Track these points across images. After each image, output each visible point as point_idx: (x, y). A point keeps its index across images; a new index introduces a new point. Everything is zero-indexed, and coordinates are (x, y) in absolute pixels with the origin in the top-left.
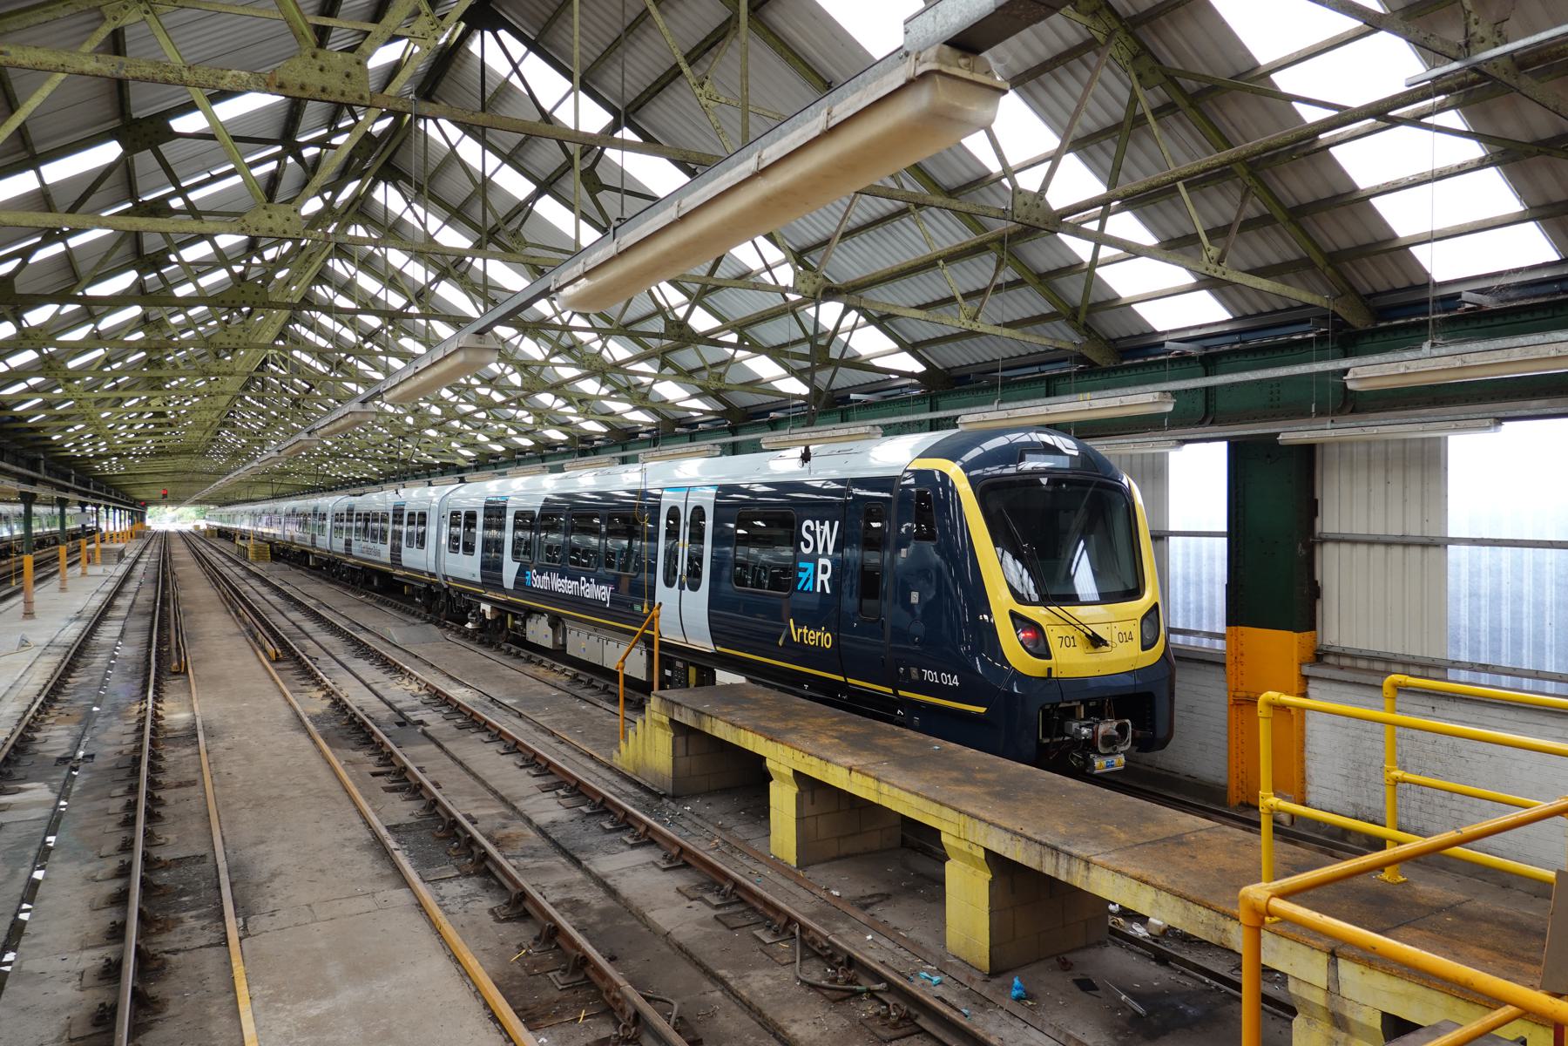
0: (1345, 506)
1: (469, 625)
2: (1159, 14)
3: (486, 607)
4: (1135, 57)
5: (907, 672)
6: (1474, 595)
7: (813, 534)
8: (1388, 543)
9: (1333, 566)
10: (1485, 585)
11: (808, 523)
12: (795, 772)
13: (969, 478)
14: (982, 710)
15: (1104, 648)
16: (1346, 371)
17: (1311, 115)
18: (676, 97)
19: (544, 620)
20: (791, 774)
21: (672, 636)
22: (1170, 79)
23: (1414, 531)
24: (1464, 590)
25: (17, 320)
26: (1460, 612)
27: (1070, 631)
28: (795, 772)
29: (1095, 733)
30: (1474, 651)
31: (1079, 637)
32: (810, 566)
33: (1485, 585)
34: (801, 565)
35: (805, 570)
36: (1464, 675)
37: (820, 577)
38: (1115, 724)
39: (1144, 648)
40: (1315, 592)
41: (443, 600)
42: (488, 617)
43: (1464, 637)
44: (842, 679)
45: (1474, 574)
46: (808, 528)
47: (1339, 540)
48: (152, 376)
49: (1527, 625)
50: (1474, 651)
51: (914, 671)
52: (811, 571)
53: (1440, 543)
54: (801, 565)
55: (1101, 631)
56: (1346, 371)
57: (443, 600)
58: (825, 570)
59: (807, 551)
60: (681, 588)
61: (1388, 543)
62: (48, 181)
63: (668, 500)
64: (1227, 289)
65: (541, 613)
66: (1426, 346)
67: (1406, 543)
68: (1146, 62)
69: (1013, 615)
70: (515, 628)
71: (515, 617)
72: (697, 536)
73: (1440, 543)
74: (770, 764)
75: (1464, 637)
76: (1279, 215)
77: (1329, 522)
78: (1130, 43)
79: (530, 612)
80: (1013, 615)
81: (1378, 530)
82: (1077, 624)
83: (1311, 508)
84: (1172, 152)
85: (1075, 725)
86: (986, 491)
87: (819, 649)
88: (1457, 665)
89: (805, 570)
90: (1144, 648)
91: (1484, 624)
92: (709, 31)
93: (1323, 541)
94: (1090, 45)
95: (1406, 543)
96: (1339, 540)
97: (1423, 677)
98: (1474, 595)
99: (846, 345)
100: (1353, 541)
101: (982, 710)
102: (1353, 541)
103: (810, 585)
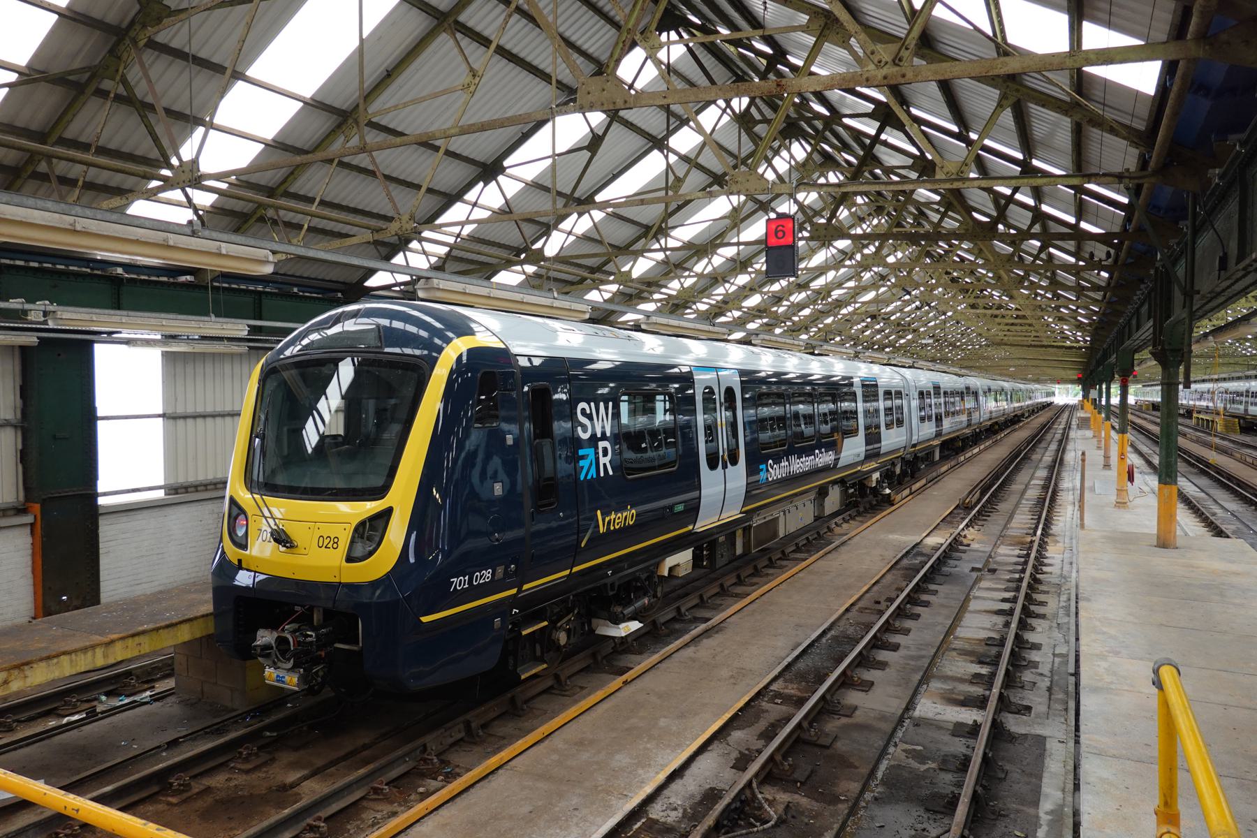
7: (590, 417)
11: (583, 405)
18: (527, 29)
25: (1079, 220)
35: (583, 457)
37: (603, 460)
39: (350, 559)
44: (567, 572)
46: (583, 410)
48: (1036, 257)
52: (592, 457)
54: (581, 452)
55: (293, 530)
58: (605, 454)
60: (725, 467)
62: (162, 483)
63: (701, 378)
72: (731, 406)
89: (583, 457)
90: (350, 559)
101: (524, 633)
103: (593, 471)
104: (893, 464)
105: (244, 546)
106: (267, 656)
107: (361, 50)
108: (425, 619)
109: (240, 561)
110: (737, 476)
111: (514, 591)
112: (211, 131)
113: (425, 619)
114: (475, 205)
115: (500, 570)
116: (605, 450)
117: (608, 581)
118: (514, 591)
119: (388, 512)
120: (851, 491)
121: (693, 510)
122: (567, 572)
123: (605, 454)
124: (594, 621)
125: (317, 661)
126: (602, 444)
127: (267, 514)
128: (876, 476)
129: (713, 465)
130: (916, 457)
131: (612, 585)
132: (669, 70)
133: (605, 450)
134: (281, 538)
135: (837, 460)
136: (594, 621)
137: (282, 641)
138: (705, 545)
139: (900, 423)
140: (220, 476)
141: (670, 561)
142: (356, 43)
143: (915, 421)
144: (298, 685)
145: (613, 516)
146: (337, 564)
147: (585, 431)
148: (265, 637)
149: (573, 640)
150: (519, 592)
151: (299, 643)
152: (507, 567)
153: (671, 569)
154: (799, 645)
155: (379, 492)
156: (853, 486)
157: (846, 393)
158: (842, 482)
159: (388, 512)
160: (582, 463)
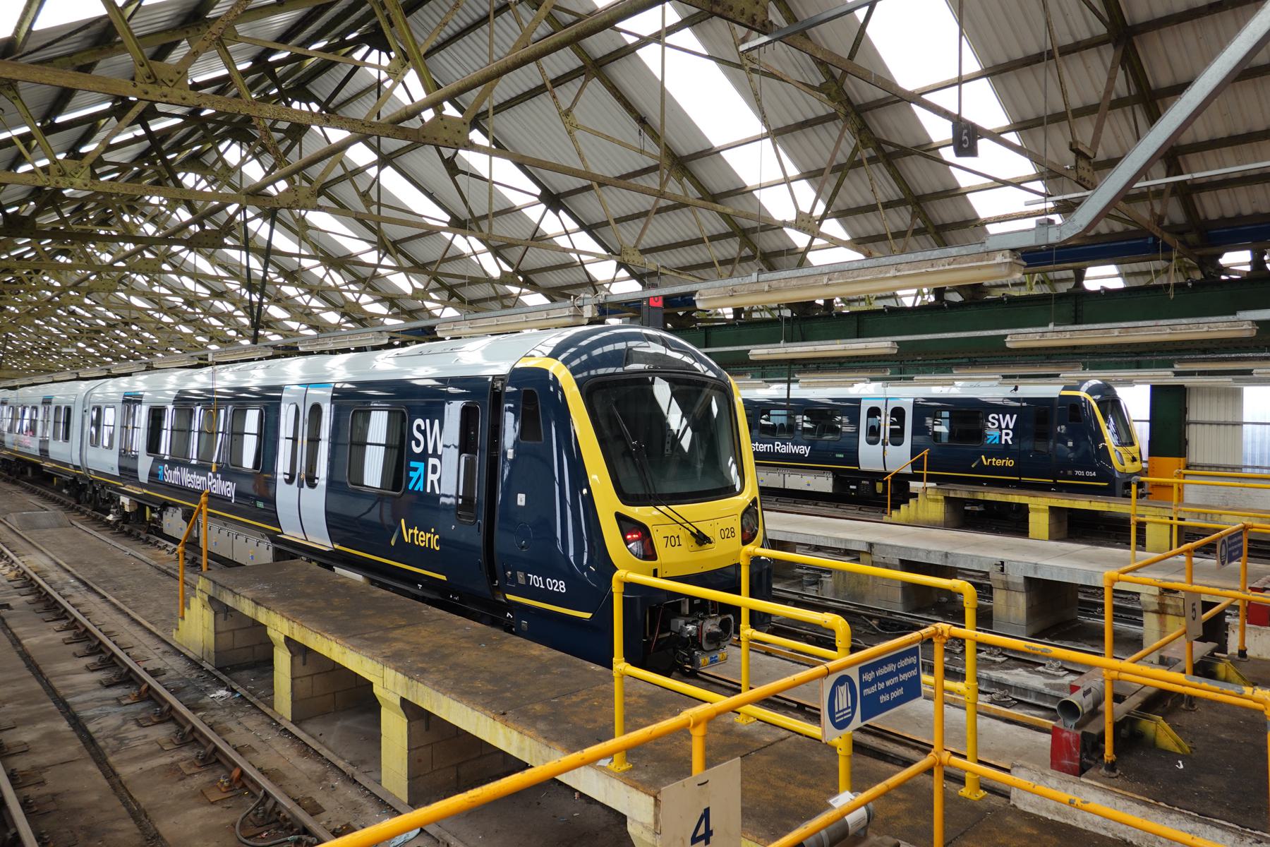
0: (1197, 410)
1: (110, 517)
2: (870, 109)
3: (125, 500)
4: (859, 130)
5: (514, 576)
6: (1253, 442)
7: (424, 433)
8: (1219, 424)
9: (1193, 433)
10: (1258, 439)
11: (419, 421)
12: (403, 700)
13: (576, 380)
14: (588, 615)
15: (708, 545)
16: (1006, 336)
17: (631, 40)
19: (179, 512)
20: (398, 702)
21: (291, 533)
22: (879, 144)
23: (1230, 420)
24: (1249, 439)
26: (1248, 448)
27: (675, 530)
28: (403, 700)
29: (699, 630)
30: (1262, 461)
31: (684, 534)
32: (421, 465)
33: (1258, 439)
34: (413, 464)
35: (415, 469)
36: (1249, 470)
38: (719, 619)
40: (1186, 442)
41: (90, 492)
42: (127, 509)
43: (1249, 457)
45: (1253, 434)
46: (419, 426)
47: (1196, 423)
49: (1257, 452)
50: (1253, 461)
51: (520, 575)
52: (421, 470)
53: (1240, 424)
54: (413, 464)
56: (1006, 336)
57: (90, 492)
58: (434, 471)
59: (418, 450)
61: (1219, 424)
64: (56, 62)
65: (175, 505)
66: (1051, 327)
67: (1226, 424)
68: (864, 133)
69: (620, 517)
70: (154, 520)
71: (152, 510)
73: (1240, 424)
74: (377, 690)
75: (1249, 457)
76: (931, 229)
77: (1192, 416)
78: (858, 121)
79: (165, 505)
80: (620, 517)
81: (1214, 419)
82: (683, 523)
83: (1185, 411)
84: (873, 185)
85: (681, 622)
86: (590, 391)
87: (427, 550)
88: (1246, 467)
89: (415, 469)
91: (1257, 452)
92: (606, 52)
93: (1189, 423)
94: (831, 118)
95: (1226, 424)
96: (1196, 423)
97: (1232, 471)
98: (1253, 442)
99: (451, 243)
100: (1203, 423)
101: (588, 615)
102: (1203, 423)
103: (997, 441)
107: (720, 61)
108: (444, 578)
112: (964, 86)
113: (444, 578)
114: (567, 233)
116: (434, 467)
123: (434, 471)
132: (250, 300)
140: (1030, 535)
142: (712, 63)
147: (418, 444)
157: (789, 430)
160: (412, 474)
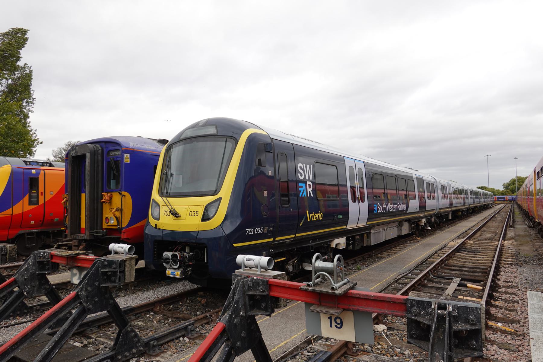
7: (303, 170)
35: (302, 187)
44: (293, 236)
46: (300, 167)
52: (304, 187)
55: (179, 210)
58: (310, 187)
60: (359, 202)
89: (302, 187)
104: (431, 217)
105: (158, 219)
106: (168, 263)
108: (235, 245)
109: (156, 225)
110: (364, 206)
111: (272, 240)
113: (235, 245)
115: (266, 229)
117: (310, 245)
118: (272, 240)
119: (220, 199)
120: (413, 225)
121: (345, 221)
122: (293, 236)
124: (304, 264)
125: (188, 266)
126: (308, 183)
127: (168, 205)
128: (424, 220)
129: (354, 201)
130: (441, 215)
131: (312, 247)
133: (309, 185)
134: (175, 214)
135: (407, 208)
136: (304, 264)
137: (174, 256)
138: (351, 235)
139: (434, 198)
141: (336, 241)
143: (440, 198)
144: (181, 276)
145: (313, 214)
146: (198, 223)
147: (301, 175)
148: (168, 254)
149: (295, 271)
150: (274, 240)
151: (181, 257)
152: (269, 228)
153: (336, 245)
154: (362, 178)
155: (216, 193)
156: (414, 223)
158: (408, 220)
159: (220, 199)
